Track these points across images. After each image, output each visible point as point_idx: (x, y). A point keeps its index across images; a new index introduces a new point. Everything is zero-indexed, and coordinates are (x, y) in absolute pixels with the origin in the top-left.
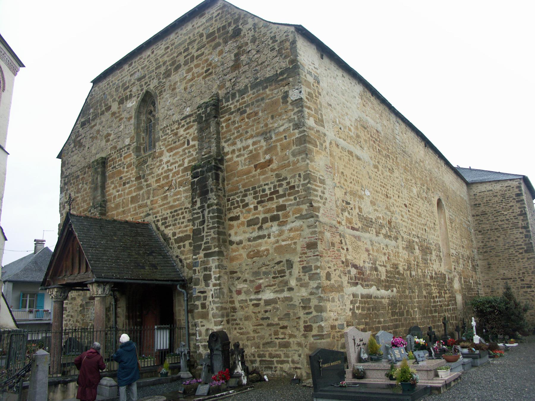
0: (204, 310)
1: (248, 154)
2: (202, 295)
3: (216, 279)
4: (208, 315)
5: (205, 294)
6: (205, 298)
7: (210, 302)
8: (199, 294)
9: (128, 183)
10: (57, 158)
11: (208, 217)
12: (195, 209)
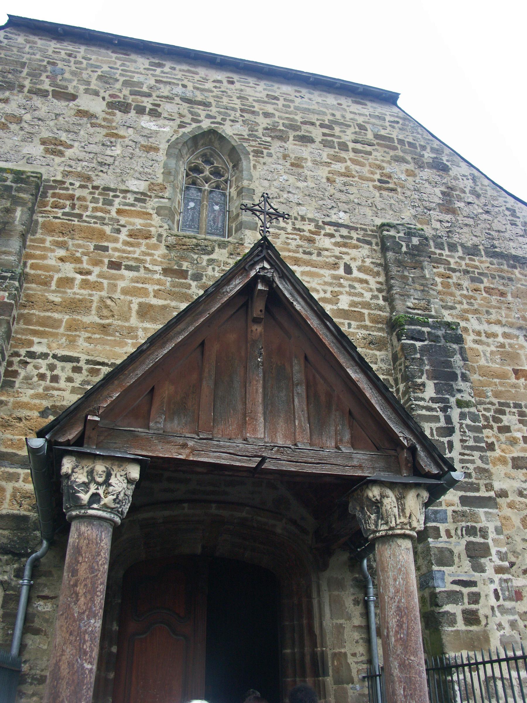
0: (474, 628)
1: (497, 347)
2: (466, 591)
3: (502, 557)
4: (487, 640)
5: (474, 589)
6: (475, 598)
7: (493, 608)
8: (457, 588)
9: (136, 269)
10: (398, 94)
11: (461, 424)
12: (423, 399)
